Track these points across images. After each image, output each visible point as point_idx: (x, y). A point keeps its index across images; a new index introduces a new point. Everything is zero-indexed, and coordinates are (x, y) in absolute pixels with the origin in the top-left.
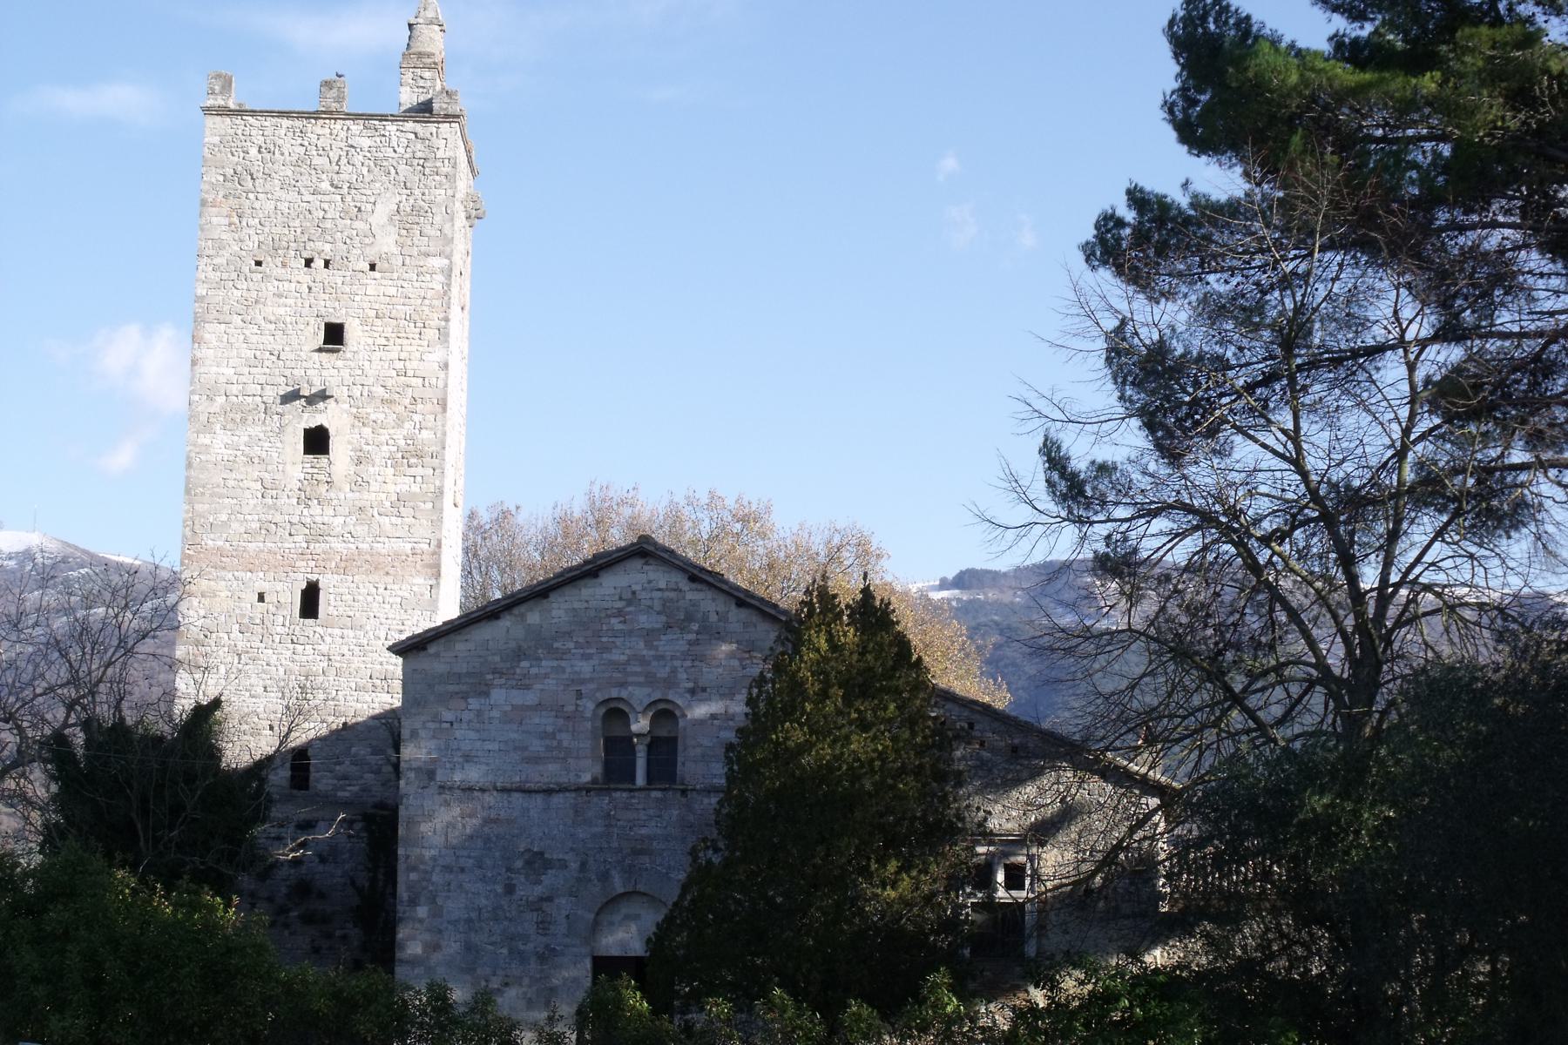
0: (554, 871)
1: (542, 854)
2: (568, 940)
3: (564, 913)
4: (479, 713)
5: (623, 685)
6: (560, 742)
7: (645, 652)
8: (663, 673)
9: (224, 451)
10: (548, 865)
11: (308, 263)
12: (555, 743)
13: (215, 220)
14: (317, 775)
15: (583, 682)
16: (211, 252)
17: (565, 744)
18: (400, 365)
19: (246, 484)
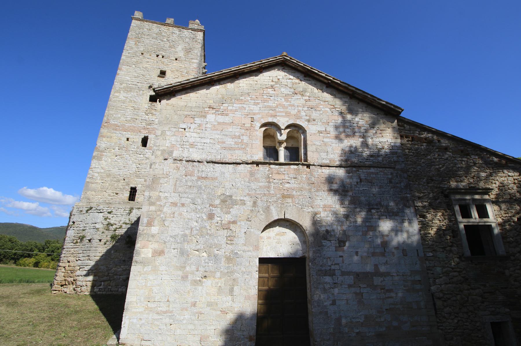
0: (238, 206)
1: (231, 196)
2: (246, 248)
3: (243, 231)
4: (200, 125)
5: (275, 116)
6: (242, 140)
7: (285, 103)
8: (294, 112)
9: (123, 98)
11: (157, 56)
12: (240, 141)
13: (131, 42)
16: (128, 49)
17: (245, 141)
19: (128, 107)
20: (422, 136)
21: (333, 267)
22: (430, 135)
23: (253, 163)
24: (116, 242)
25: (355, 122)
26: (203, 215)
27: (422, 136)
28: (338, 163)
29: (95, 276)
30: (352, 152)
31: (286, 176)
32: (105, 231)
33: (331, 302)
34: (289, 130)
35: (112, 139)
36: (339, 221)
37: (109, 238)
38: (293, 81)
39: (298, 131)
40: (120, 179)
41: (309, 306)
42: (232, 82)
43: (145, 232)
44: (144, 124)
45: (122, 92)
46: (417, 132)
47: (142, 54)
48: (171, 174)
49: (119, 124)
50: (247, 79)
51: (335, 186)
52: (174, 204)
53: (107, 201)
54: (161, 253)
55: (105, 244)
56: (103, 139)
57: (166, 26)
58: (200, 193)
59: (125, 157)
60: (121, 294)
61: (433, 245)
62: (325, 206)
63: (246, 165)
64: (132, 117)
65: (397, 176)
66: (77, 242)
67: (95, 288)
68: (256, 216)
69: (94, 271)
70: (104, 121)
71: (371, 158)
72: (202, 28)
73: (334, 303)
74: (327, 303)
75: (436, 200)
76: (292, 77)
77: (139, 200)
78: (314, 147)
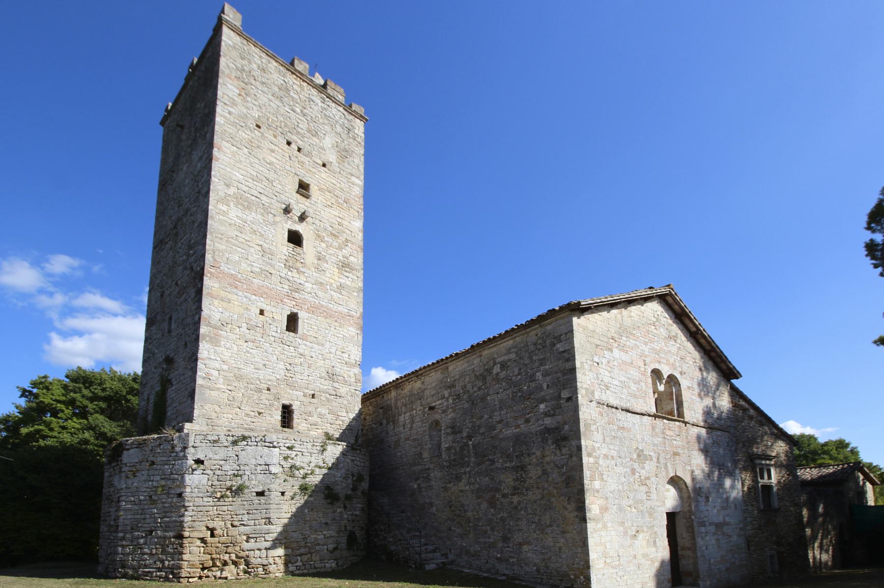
18: (340, 220)
24: (310, 496)
29: (286, 548)
37: (296, 488)
40: (261, 387)
44: (287, 287)
49: (239, 276)
53: (245, 426)
55: (292, 499)
56: (213, 302)
57: (294, 76)
59: (262, 346)
60: (330, 570)
69: (284, 541)
76: (667, 316)
77: (300, 427)
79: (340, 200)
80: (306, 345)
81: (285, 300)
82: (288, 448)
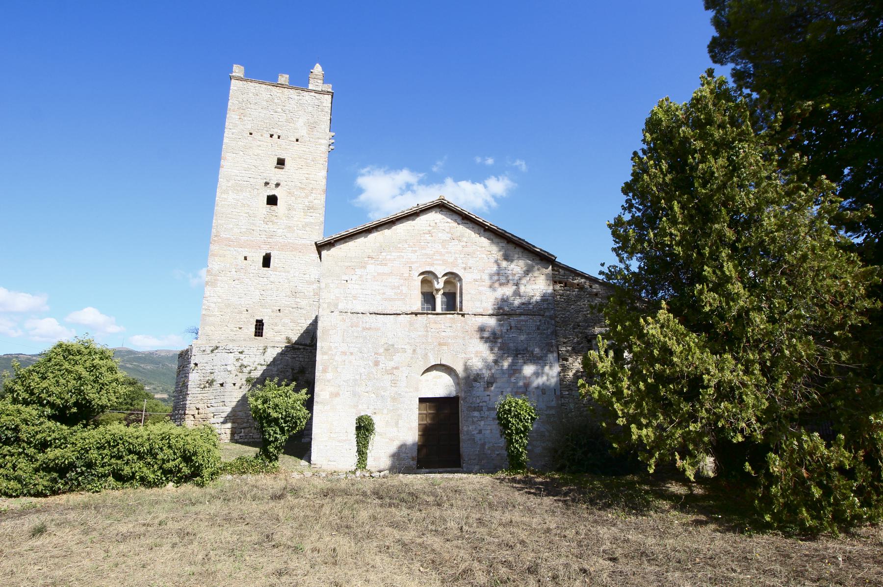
0: (399, 354)
1: (393, 345)
3: (405, 375)
4: (361, 276)
5: (432, 265)
7: (442, 250)
8: (451, 260)
10: (397, 351)
11: (271, 136)
12: (399, 291)
13: (234, 116)
14: (267, 331)
15: (413, 263)
16: (231, 127)
18: (307, 176)
19: (241, 214)
20: (575, 282)
21: (481, 404)
22: (583, 280)
23: (412, 313)
25: (510, 269)
26: (370, 362)
27: (575, 282)
28: (491, 312)
29: (233, 423)
30: (504, 300)
31: (443, 325)
32: (238, 373)
33: (477, 432)
34: (446, 277)
35: (226, 258)
36: (489, 367)
38: (451, 225)
39: (455, 279)
41: (460, 435)
42: (389, 228)
43: (321, 377)
44: (264, 236)
45: (230, 192)
46: (571, 277)
47: (251, 134)
48: (338, 325)
49: (232, 237)
50: (404, 224)
51: (486, 335)
52: (344, 353)
53: (230, 338)
54: (337, 395)
57: (278, 88)
58: (366, 343)
61: (570, 385)
62: (477, 352)
63: (406, 316)
64: (248, 227)
65: (545, 323)
66: (205, 387)
67: (236, 435)
68: (416, 362)
70: (212, 234)
71: (524, 306)
72: (328, 88)
73: (480, 432)
74: (475, 432)
75: (580, 344)
76: (449, 220)
77: (268, 335)
78: (469, 295)
79: (308, 161)
80: (275, 274)
81: (262, 246)
82: (239, 353)
